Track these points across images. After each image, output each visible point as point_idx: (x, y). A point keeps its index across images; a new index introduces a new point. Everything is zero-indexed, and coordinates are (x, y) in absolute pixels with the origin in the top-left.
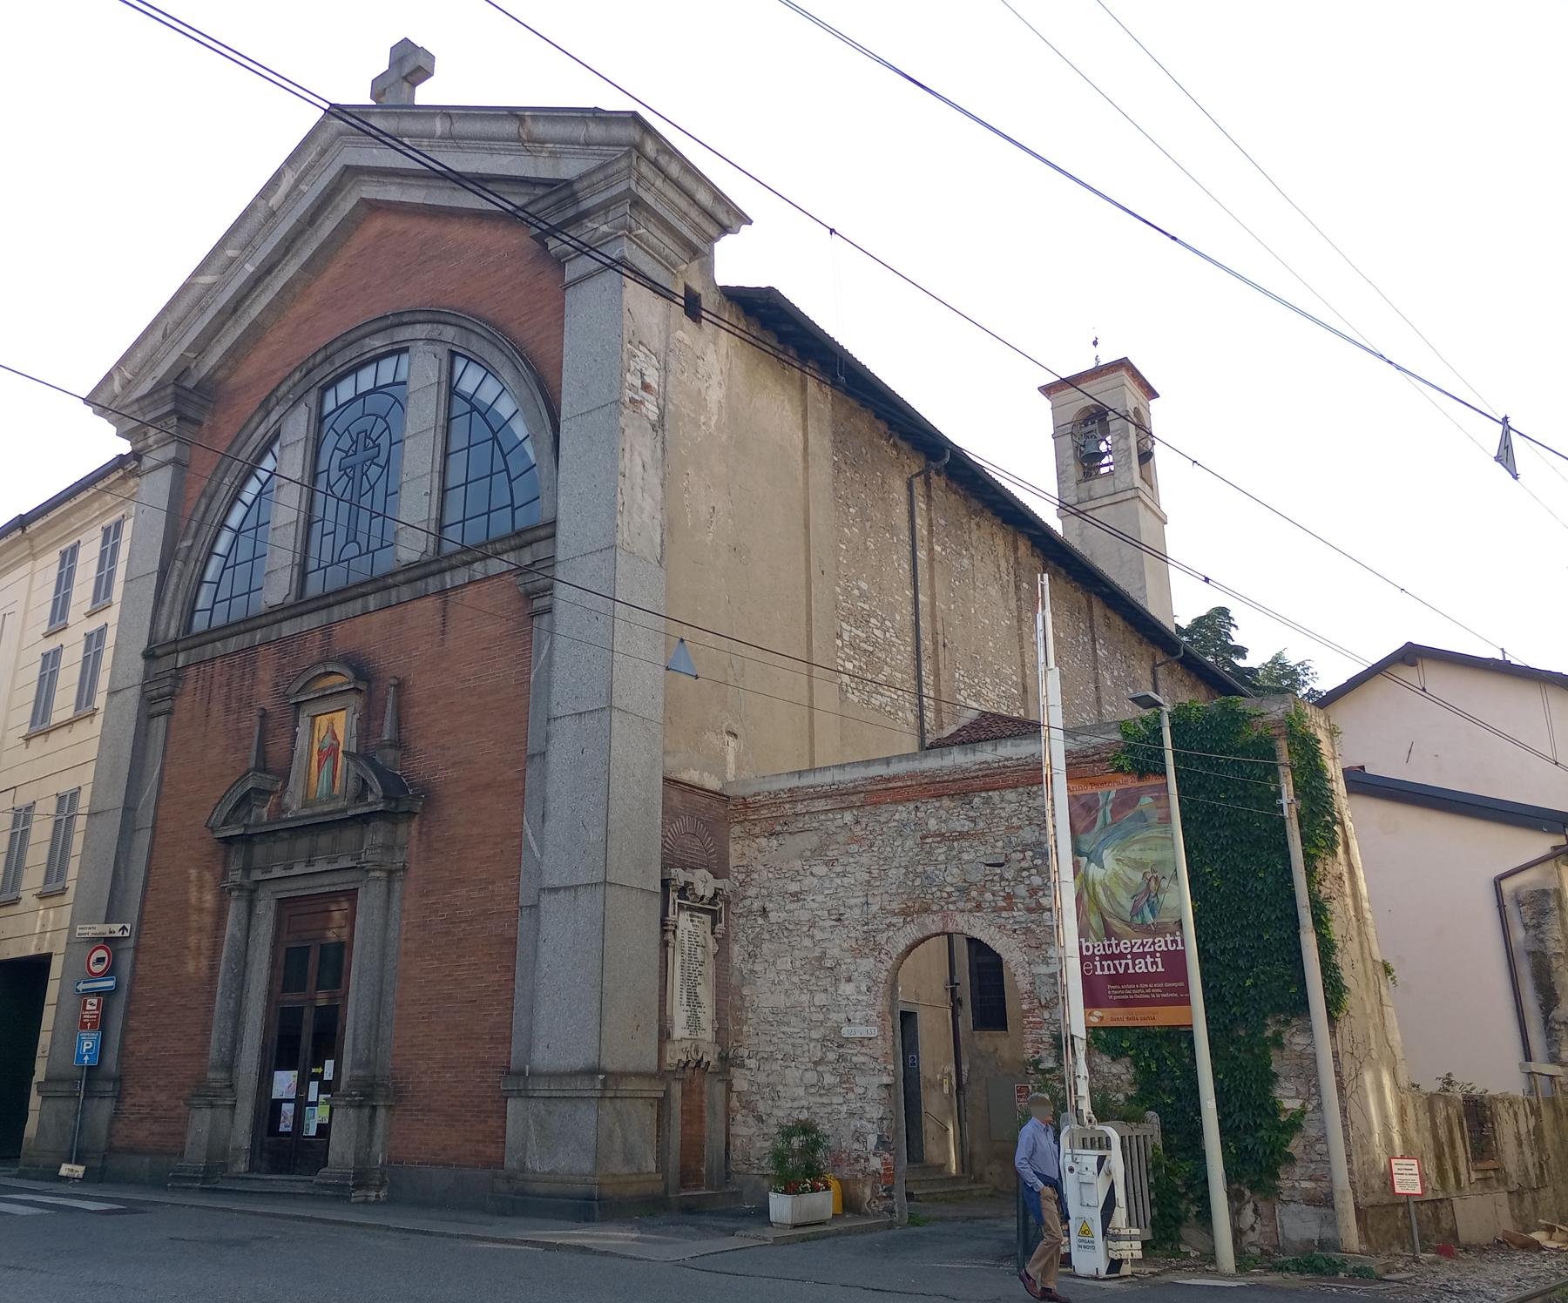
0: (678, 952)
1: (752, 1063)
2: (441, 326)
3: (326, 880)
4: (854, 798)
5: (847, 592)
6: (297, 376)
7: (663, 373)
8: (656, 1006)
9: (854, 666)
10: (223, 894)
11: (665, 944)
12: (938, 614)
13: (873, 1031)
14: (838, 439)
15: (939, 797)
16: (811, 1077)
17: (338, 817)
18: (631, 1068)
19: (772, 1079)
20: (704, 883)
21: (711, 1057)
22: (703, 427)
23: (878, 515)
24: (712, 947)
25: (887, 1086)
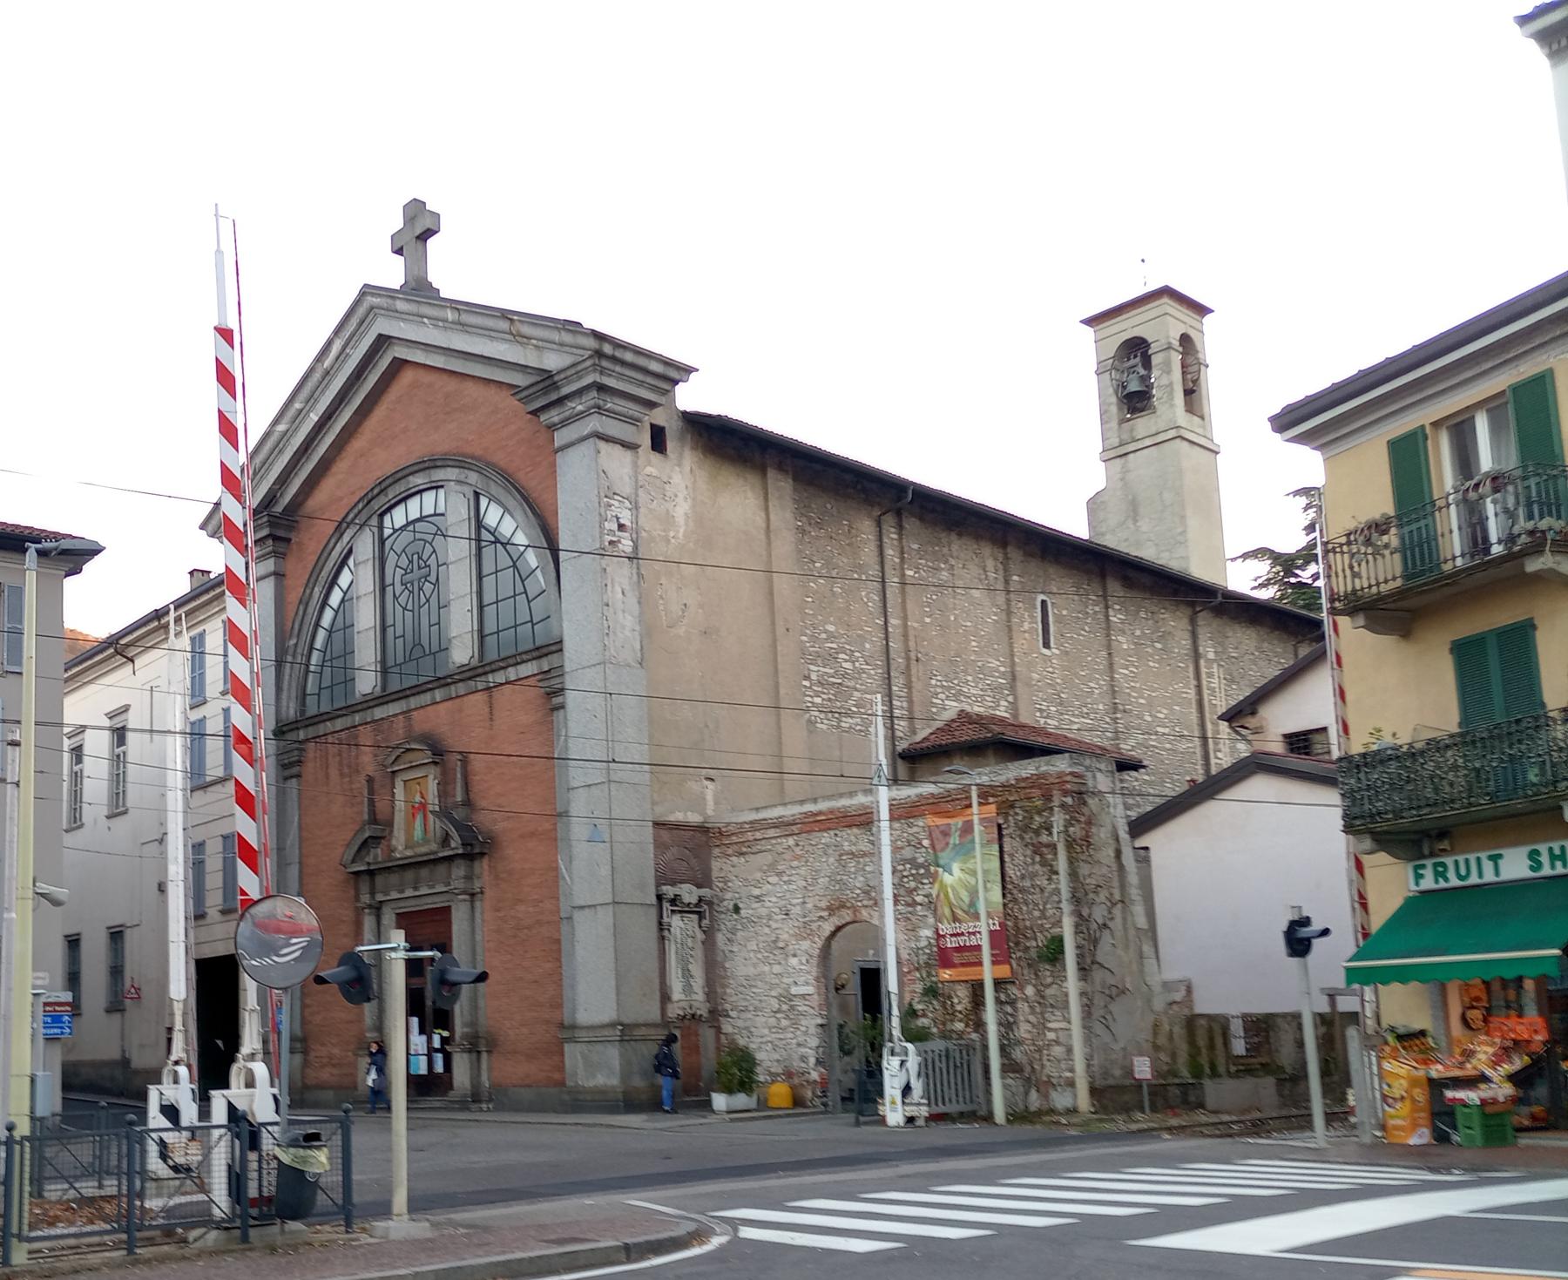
0: (673, 942)
1: (733, 1014)
2: (466, 471)
3: (429, 900)
4: (794, 828)
5: (814, 639)
6: (360, 506)
7: (634, 512)
8: (657, 981)
9: (823, 699)
10: (359, 913)
11: (663, 938)
12: (911, 633)
13: (810, 990)
14: (802, 505)
15: (850, 826)
16: (772, 1021)
17: (432, 857)
18: (641, 1021)
19: (748, 1024)
20: (689, 894)
21: (703, 1011)
22: (673, 541)
23: (845, 560)
24: (700, 936)
25: (822, 1025)
